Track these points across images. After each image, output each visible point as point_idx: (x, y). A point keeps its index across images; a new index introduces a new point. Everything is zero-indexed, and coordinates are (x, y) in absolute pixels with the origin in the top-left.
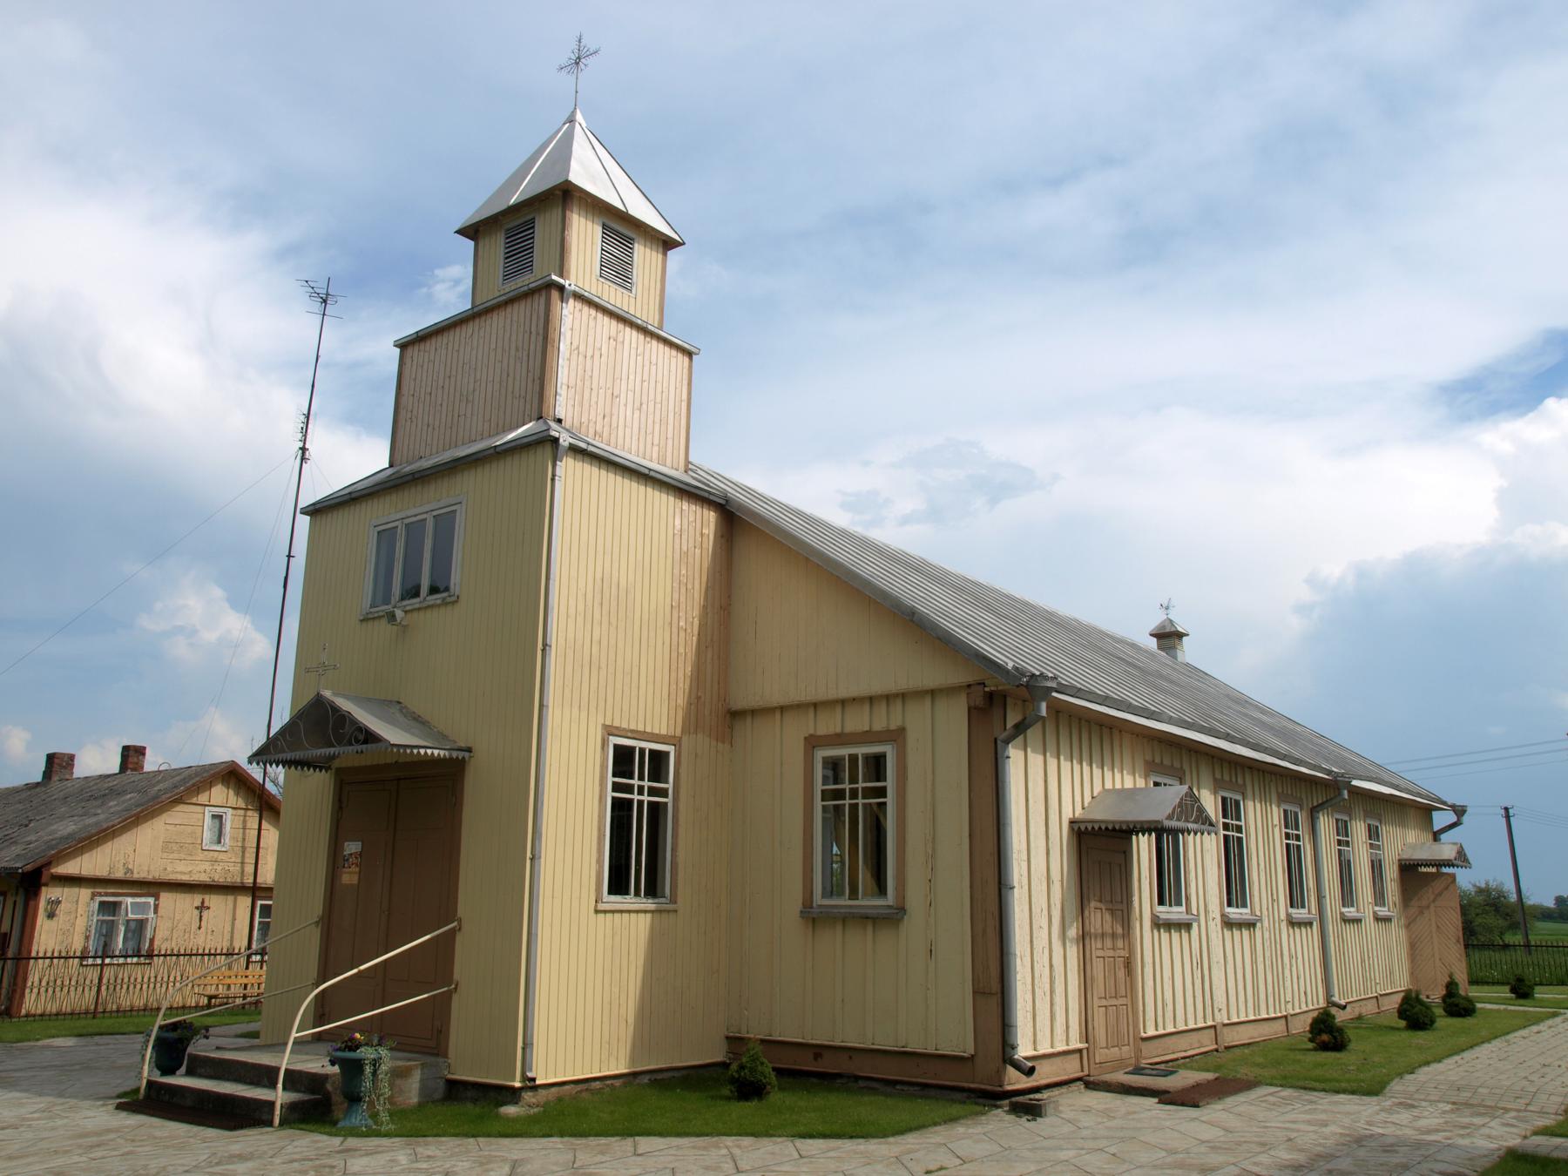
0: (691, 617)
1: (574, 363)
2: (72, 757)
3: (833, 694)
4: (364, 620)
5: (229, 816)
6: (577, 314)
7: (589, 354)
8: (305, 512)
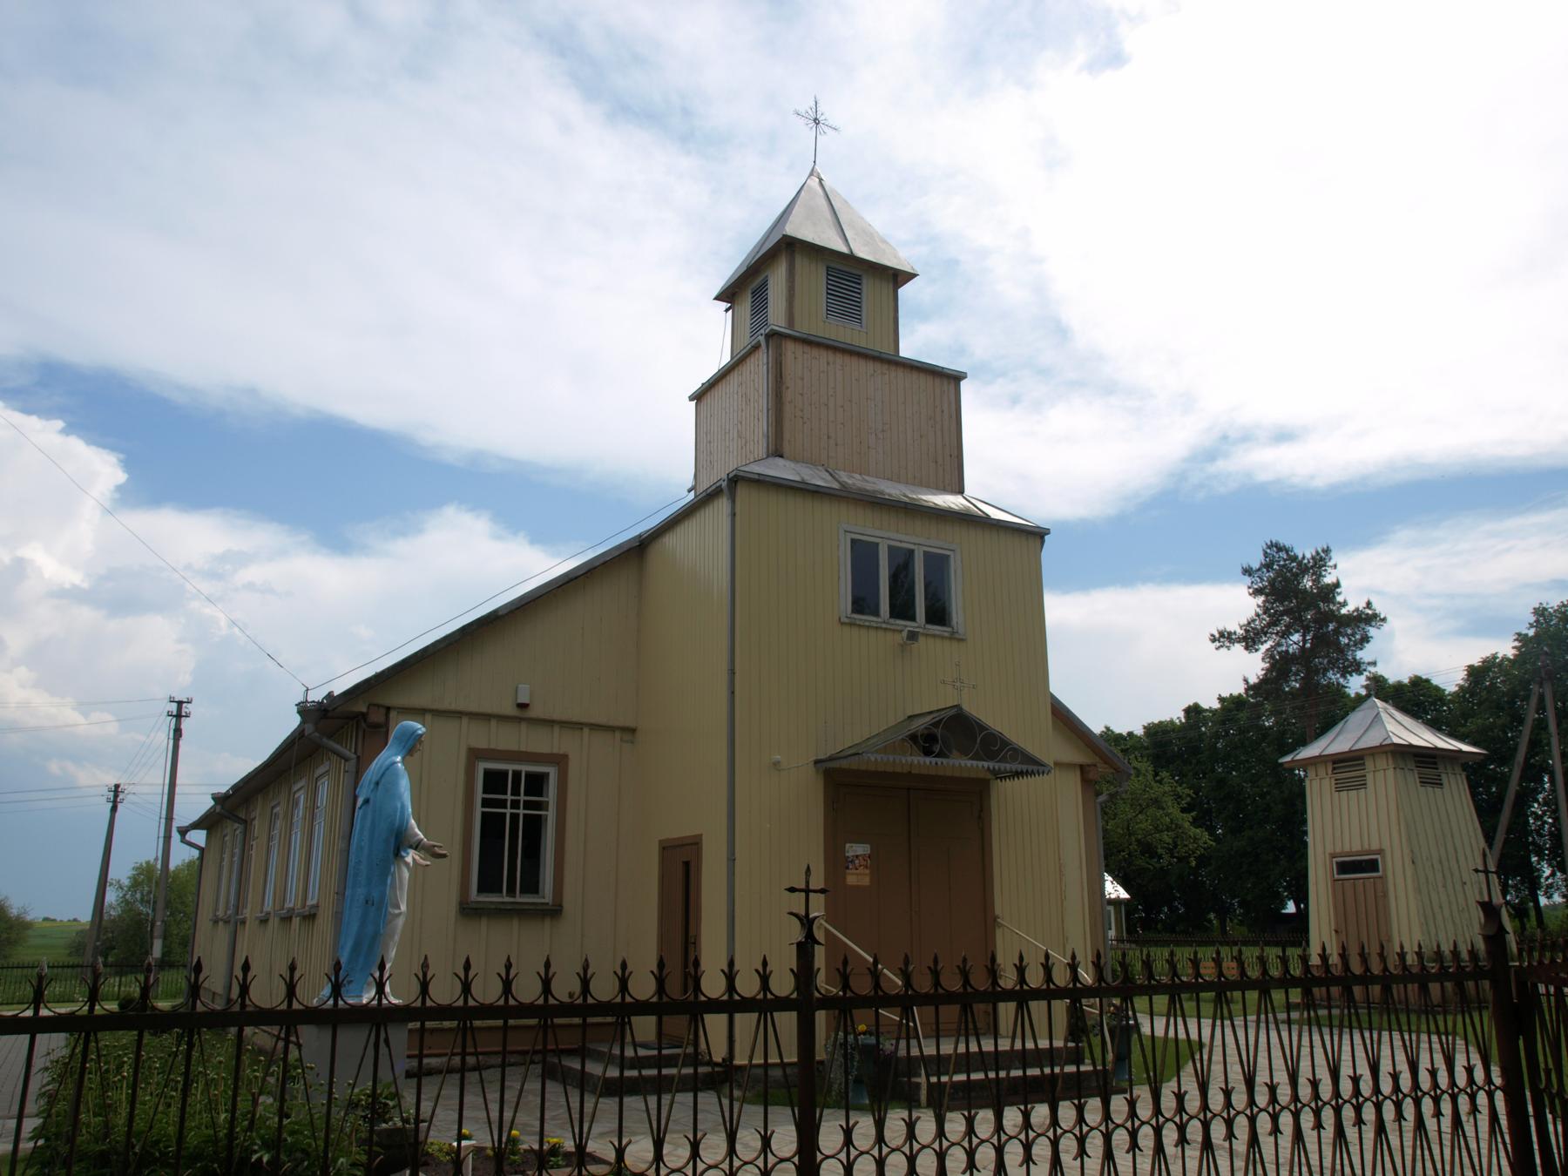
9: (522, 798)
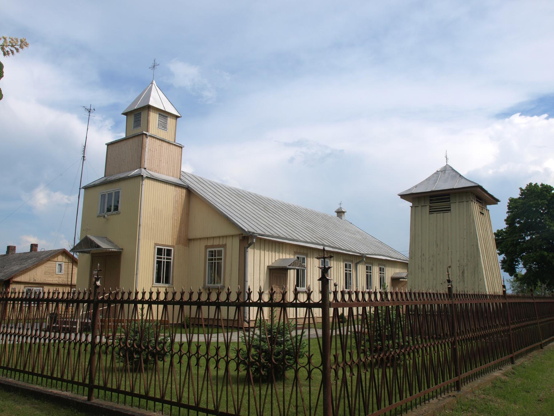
0: (178, 217)
1: (149, 153)
2: (15, 247)
3: (211, 236)
4: (97, 217)
5: (63, 265)
6: (150, 141)
7: (154, 150)
8: (83, 188)
9: (165, 257)
